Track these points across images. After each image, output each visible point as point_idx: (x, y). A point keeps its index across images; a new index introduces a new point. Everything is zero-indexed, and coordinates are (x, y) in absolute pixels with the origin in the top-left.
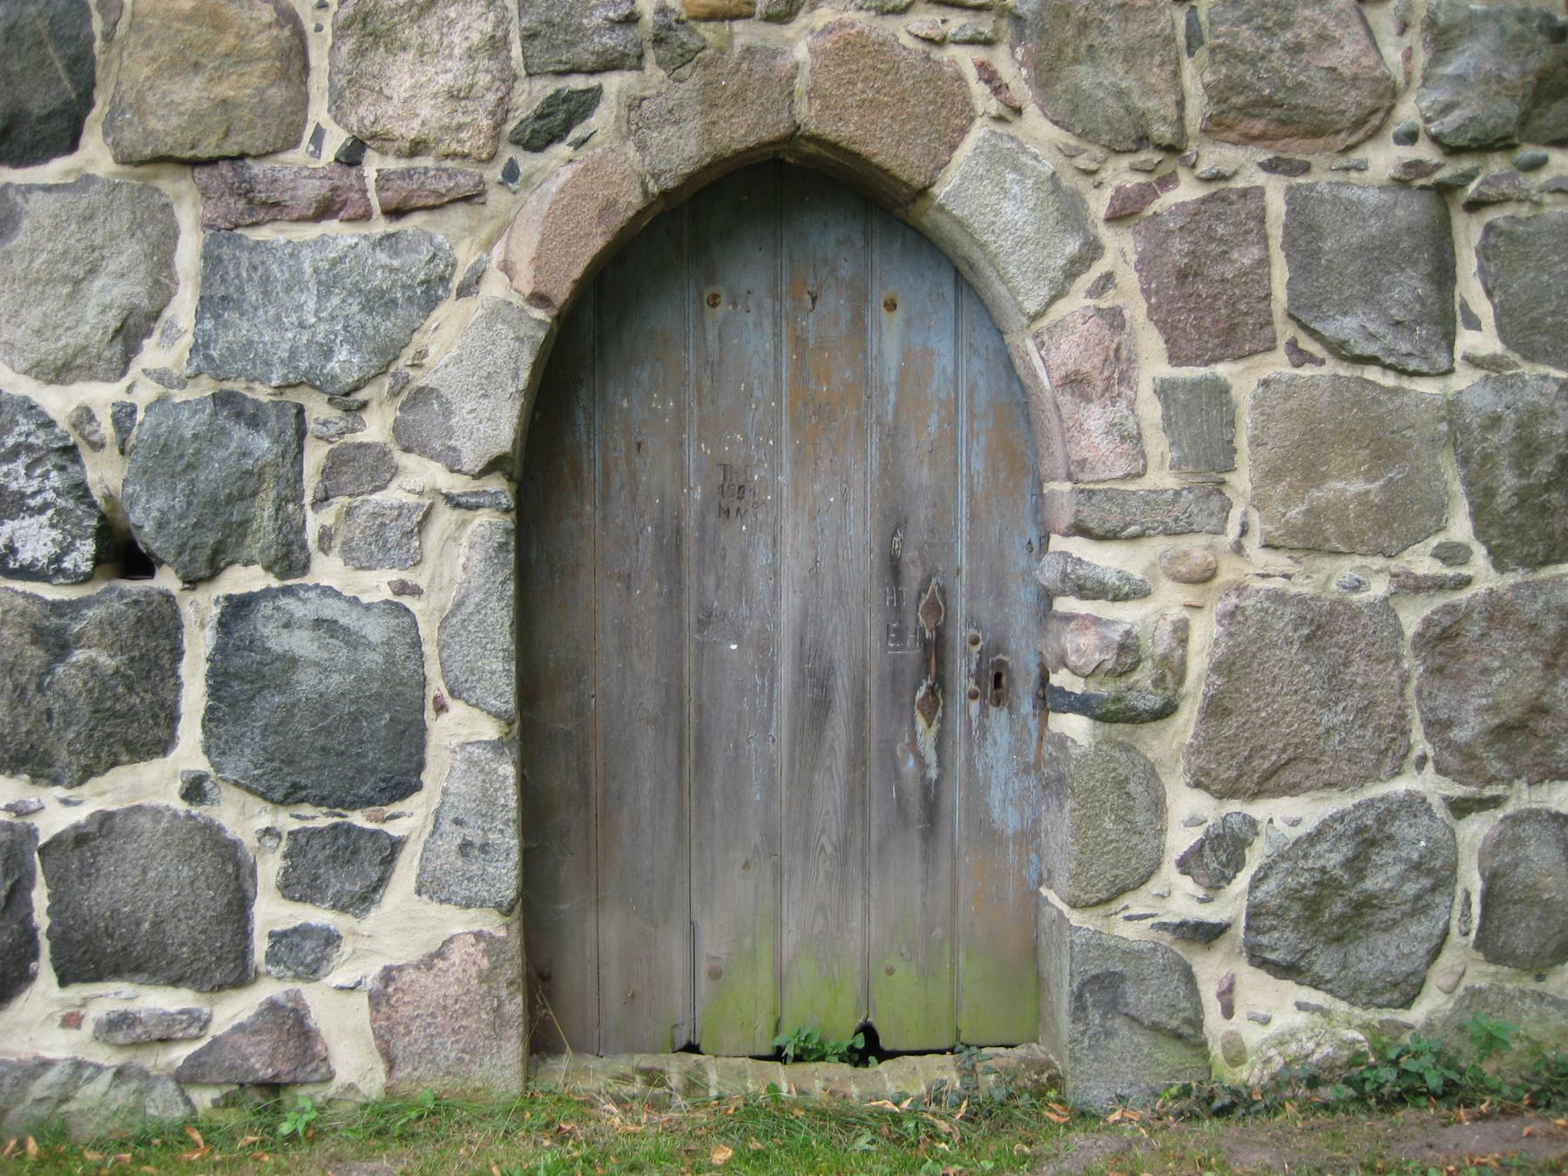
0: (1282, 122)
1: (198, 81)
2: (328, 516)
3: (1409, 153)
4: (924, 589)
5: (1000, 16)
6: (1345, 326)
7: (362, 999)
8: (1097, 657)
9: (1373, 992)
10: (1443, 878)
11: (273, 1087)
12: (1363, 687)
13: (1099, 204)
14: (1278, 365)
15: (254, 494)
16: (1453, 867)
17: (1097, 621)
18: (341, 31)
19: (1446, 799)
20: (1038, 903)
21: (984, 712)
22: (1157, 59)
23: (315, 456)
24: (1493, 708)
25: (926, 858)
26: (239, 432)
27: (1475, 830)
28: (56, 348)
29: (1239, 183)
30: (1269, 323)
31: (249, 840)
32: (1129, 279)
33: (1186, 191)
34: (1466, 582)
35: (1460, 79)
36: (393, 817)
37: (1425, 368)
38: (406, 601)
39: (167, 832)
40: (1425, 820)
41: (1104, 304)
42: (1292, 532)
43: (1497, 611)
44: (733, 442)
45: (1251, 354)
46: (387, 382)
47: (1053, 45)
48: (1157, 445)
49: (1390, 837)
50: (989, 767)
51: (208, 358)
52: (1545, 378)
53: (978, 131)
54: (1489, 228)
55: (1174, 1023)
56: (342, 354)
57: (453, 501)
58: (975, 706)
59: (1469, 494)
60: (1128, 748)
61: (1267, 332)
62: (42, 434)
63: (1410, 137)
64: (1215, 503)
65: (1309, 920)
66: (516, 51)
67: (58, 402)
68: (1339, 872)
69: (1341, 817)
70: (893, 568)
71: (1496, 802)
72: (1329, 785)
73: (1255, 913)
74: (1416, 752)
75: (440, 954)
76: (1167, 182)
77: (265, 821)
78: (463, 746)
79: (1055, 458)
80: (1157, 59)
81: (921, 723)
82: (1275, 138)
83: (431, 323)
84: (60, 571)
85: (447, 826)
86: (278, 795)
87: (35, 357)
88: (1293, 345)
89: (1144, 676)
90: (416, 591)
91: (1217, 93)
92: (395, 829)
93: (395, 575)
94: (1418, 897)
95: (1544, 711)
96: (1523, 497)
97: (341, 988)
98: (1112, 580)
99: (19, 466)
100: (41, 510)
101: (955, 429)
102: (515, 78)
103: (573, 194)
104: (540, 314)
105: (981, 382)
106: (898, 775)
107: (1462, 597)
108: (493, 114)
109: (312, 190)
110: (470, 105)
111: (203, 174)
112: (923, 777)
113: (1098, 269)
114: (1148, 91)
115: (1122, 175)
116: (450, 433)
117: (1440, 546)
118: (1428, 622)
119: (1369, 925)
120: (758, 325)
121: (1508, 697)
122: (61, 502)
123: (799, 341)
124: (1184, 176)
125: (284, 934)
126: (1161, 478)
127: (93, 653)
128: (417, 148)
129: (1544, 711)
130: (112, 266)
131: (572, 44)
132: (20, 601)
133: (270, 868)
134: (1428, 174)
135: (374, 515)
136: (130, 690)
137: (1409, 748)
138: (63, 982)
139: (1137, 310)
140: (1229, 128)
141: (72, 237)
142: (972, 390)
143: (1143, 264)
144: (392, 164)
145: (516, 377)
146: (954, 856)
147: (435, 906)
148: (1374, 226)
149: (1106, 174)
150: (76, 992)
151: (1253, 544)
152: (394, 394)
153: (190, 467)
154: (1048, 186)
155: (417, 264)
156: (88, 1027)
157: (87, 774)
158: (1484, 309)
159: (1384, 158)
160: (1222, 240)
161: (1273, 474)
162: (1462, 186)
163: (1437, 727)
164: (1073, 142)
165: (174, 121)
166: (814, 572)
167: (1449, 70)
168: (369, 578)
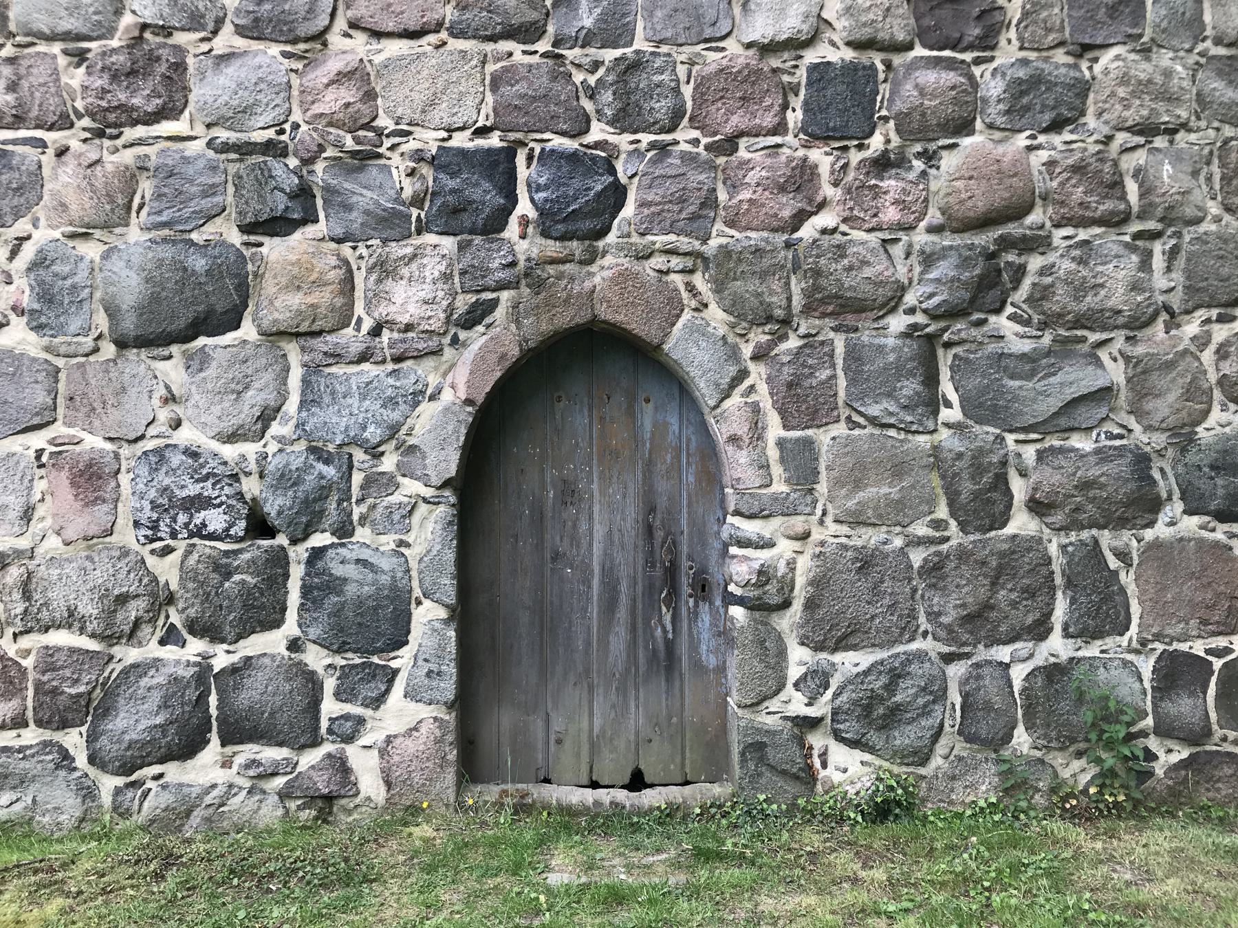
0: (842, 306)
1: (300, 295)
2: (363, 508)
3: (911, 320)
4: (664, 542)
5: (697, 258)
6: (874, 410)
7: (376, 752)
8: (747, 577)
9: (903, 757)
10: (941, 695)
11: (329, 799)
12: (891, 594)
13: (747, 350)
14: (840, 429)
15: (327, 497)
16: (945, 690)
17: (747, 559)
18: (370, 270)
19: (939, 653)
20: (726, 703)
21: (696, 605)
22: (777, 277)
23: (357, 478)
24: (964, 606)
25: (667, 680)
26: (320, 466)
27: (956, 671)
28: (228, 425)
29: (820, 338)
30: (836, 408)
31: (321, 671)
32: (763, 388)
33: (793, 343)
34: (947, 539)
35: (938, 281)
36: (394, 658)
37: (921, 429)
38: (403, 550)
39: (278, 666)
40: (927, 665)
41: (749, 400)
42: (848, 512)
43: (963, 554)
44: (568, 469)
45: (827, 424)
46: (394, 442)
47: (724, 271)
48: (777, 470)
49: (909, 673)
50: (699, 633)
51: (304, 430)
52: (987, 433)
53: (687, 316)
54: (955, 356)
55: (794, 770)
56: (371, 428)
57: (425, 500)
58: (691, 601)
59: (946, 494)
60: (766, 624)
61: (835, 413)
62: (221, 467)
63: (911, 311)
64: (809, 499)
65: (866, 716)
66: (457, 280)
67: (230, 452)
68: (880, 692)
69: (882, 662)
70: (649, 530)
71: (968, 656)
72: (874, 645)
73: (835, 712)
74: (922, 629)
75: (416, 729)
76: (784, 337)
77: (328, 661)
78: (429, 622)
79: (726, 480)
80: (777, 277)
81: (664, 609)
82: (839, 314)
83: (416, 413)
84: (228, 536)
85: (420, 662)
86: (335, 647)
87: (219, 430)
88: (849, 418)
89: (771, 588)
90: (408, 545)
91: (808, 294)
92: (394, 664)
93: (397, 537)
94: (925, 706)
95: (992, 608)
96: (976, 495)
97: (365, 747)
98: (754, 538)
99: (209, 484)
100: (219, 505)
101: (680, 461)
102: (457, 293)
103: (481, 357)
104: (470, 409)
105: (693, 438)
106: (653, 636)
107: (944, 547)
108: (445, 311)
109: (356, 348)
110: (435, 307)
111: (302, 341)
112: (665, 638)
113: (747, 383)
114: (772, 293)
115: (759, 336)
116: (425, 467)
117: (931, 521)
118: (925, 560)
119: (900, 720)
120: (581, 411)
121: (971, 600)
122: (230, 502)
123: (602, 419)
124: (791, 334)
125: (337, 719)
126: (780, 487)
127: (244, 577)
128: (409, 328)
129: (992, 608)
130: (256, 385)
131: (484, 277)
132: (208, 551)
133: (330, 685)
134: (922, 330)
135: (387, 508)
136: (262, 594)
137: (918, 626)
138: (223, 745)
139: (766, 404)
140: (815, 310)
141: (236, 372)
142: (689, 440)
143: (769, 380)
144: (396, 335)
145: (458, 440)
146: (682, 681)
147: (414, 704)
148: (892, 358)
149: (751, 336)
150: (229, 750)
151: (829, 520)
152: (397, 448)
153: (295, 484)
154: (721, 343)
155: (408, 383)
156: (235, 768)
157: (240, 637)
158: (953, 397)
159: (897, 323)
160: (811, 367)
161: (837, 483)
162: (941, 336)
163: (933, 616)
164: (732, 319)
165: (288, 315)
166: (610, 533)
167: (931, 276)
168: (383, 538)
